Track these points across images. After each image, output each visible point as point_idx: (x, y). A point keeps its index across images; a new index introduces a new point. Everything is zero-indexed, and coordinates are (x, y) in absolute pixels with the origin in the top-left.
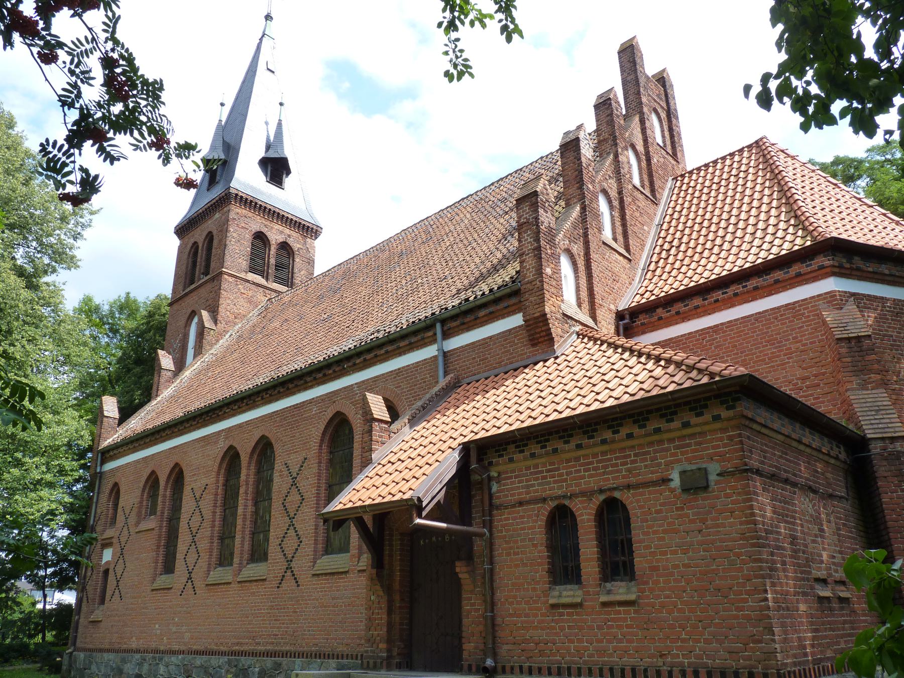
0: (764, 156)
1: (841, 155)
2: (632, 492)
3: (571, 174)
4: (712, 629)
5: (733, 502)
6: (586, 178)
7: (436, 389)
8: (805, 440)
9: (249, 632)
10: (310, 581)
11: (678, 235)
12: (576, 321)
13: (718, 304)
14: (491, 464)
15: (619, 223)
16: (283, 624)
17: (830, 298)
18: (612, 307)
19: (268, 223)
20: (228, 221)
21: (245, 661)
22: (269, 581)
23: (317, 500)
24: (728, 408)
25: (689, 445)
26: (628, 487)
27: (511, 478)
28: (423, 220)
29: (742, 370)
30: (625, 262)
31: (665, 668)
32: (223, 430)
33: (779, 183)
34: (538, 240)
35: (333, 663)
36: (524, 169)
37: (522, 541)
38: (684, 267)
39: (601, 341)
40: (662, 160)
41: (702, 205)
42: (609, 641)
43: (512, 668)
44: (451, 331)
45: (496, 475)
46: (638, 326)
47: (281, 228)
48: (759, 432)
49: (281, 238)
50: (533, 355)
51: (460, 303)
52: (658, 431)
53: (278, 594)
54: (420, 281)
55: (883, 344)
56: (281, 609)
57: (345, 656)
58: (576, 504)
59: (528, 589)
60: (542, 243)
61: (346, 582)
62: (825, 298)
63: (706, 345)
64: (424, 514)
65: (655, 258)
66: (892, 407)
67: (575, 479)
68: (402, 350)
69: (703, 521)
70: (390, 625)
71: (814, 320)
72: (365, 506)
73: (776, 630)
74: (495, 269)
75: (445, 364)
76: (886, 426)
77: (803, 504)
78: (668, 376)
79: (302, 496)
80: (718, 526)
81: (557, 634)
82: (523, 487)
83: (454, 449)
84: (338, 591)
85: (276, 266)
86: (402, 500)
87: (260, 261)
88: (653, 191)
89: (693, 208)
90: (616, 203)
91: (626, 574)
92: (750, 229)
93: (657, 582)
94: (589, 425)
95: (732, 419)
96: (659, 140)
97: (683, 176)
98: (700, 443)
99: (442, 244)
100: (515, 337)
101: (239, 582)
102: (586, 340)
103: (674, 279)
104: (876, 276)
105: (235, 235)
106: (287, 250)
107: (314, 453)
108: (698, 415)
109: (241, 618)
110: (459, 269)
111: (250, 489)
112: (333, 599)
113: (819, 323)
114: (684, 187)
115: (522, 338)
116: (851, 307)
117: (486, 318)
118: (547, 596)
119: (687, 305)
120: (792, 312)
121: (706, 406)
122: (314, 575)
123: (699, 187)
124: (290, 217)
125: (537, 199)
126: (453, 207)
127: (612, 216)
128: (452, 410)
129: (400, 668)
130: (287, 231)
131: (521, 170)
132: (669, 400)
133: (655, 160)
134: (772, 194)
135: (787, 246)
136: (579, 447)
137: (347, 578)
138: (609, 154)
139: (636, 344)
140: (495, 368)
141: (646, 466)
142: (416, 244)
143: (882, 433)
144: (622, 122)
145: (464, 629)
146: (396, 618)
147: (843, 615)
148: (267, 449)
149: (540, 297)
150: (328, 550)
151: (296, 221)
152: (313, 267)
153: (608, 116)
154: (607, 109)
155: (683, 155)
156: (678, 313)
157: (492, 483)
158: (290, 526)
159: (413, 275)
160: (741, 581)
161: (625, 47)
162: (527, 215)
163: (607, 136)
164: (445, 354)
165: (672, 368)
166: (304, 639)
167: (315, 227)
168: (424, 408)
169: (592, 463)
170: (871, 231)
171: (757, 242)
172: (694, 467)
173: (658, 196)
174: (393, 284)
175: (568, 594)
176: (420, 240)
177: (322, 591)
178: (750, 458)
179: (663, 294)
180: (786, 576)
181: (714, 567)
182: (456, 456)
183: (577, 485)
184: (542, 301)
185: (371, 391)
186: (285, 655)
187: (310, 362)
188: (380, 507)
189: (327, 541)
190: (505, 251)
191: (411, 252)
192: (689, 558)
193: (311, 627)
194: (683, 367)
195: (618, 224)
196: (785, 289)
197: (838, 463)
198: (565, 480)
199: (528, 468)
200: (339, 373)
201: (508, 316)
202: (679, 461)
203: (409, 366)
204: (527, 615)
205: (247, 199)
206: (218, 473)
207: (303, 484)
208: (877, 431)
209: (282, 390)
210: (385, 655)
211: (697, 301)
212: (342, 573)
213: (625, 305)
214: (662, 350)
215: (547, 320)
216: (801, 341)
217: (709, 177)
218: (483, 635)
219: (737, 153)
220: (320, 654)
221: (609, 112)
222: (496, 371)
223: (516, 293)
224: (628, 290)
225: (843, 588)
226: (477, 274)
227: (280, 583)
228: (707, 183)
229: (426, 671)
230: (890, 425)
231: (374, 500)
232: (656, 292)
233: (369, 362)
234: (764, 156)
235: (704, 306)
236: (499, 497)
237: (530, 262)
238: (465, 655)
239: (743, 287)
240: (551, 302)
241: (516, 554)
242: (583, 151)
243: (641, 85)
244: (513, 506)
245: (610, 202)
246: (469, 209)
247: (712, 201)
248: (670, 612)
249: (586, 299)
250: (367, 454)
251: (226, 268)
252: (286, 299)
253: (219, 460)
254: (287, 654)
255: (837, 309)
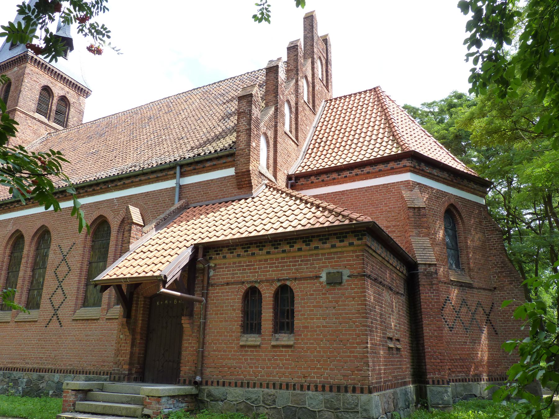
0: (378, 97)
1: (408, 104)
2: (297, 282)
3: (272, 87)
4: (335, 363)
5: (355, 293)
6: (279, 91)
7: (173, 208)
8: (391, 262)
9: (21, 355)
10: (69, 324)
11: (326, 135)
12: (266, 177)
13: (346, 179)
14: (211, 258)
15: (294, 122)
16: (48, 351)
17: (407, 184)
18: (286, 172)
19: (53, 81)
20: (24, 74)
21: (16, 374)
22: (39, 322)
23: (80, 271)
24: (358, 239)
25: (333, 258)
26: (295, 279)
27: (223, 268)
28: (166, 98)
29: (369, 219)
30: (295, 146)
31: (306, 384)
33: (385, 115)
34: (250, 124)
35: (82, 376)
36: (236, 78)
37: (226, 306)
38: (323, 156)
39: (282, 191)
40: (320, 88)
41: (341, 119)
42: (274, 368)
43: (212, 382)
44: (186, 173)
45: (213, 265)
46: (299, 185)
47: (63, 86)
48: (371, 254)
49: (62, 93)
50: (238, 195)
51: (194, 156)
52: (317, 248)
53: (46, 331)
54: (164, 137)
55: (430, 213)
56: (47, 341)
57: (92, 373)
58: (263, 287)
59: (227, 336)
60: (252, 126)
61: (97, 325)
62: (404, 184)
63: (337, 202)
64: (167, 286)
65: (311, 146)
66: (431, 248)
67: (264, 272)
68: (151, 180)
69: (337, 302)
70: (132, 354)
71: (397, 195)
72: (126, 278)
73: (370, 364)
74: (217, 138)
75: (180, 193)
76: (427, 257)
77: (387, 296)
78: (315, 218)
79: (69, 268)
80: (345, 305)
81: (242, 363)
82: (230, 274)
83: (187, 247)
84: (90, 331)
85: (56, 111)
86: (153, 276)
87: (45, 106)
88: (314, 106)
89: (336, 121)
90: (294, 110)
91: (288, 329)
92: (368, 138)
93: (307, 335)
94: (276, 241)
95: (360, 246)
96: (320, 76)
97: (331, 100)
98: (340, 258)
99: (180, 116)
100: (228, 182)
101: (16, 322)
102: (272, 189)
103: (307, 160)
104: (431, 176)
105: (28, 85)
106: (65, 102)
107: (81, 241)
108: (341, 241)
109: (16, 346)
110: (192, 133)
111: (30, 260)
112: (86, 336)
113: (399, 197)
114: (331, 107)
115: (232, 183)
116: (417, 190)
117: (210, 168)
118: (238, 340)
119: (329, 177)
120: (386, 189)
121: (346, 237)
122: (73, 320)
123: (340, 109)
124: (70, 79)
125: (251, 99)
126: (187, 93)
127: (291, 118)
128: (184, 222)
129: (136, 381)
130: (67, 89)
131: (234, 78)
132: (325, 231)
133: (317, 88)
134: (381, 120)
135: (388, 151)
136: (268, 253)
137: (98, 323)
138: (292, 79)
139: (304, 196)
140: (213, 199)
141: (307, 268)
142: (161, 113)
143: (425, 261)
144: (302, 61)
145: (183, 357)
146: (137, 349)
147: (397, 358)
148: (45, 235)
149: (247, 160)
150: (85, 304)
151: (74, 83)
152: (83, 116)
153: (295, 56)
154: (295, 51)
155: (332, 88)
156: (323, 181)
157: (210, 270)
158: (58, 287)
159: (159, 133)
160: (354, 336)
161: (308, 15)
162: (244, 107)
163: (293, 68)
164: (181, 187)
165: (326, 213)
166: (63, 361)
167: (87, 90)
168: (165, 219)
169: (275, 263)
170: (429, 150)
171: (371, 147)
172: (335, 271)
173: (316, 109)
174: (145, 137)
175: (252, 339)
176: (163, 110)
177: (78, 331)
178: (367, 269)
179: (315, 169)
180: (377, 335)
181: (340, 328)
182: (189, 252)
183: (264, 276)
184: (248, 162)
185: (135, 205)
186: (47, 371)
187: (83, 180)
188: (136, 280)
189: (85, 298)
190: (224, 127)
191: (157, 118)
192: (327, 323)
193: (68, 353)
194: (334, 213)
195: (293, 122)
196: (384, 175)
197: (402, 276)
198: (257, 272)
199: (234, 263)
200: (104, 190)
201: (228, 168)
202: (327, 267)
203: (155, 191)
204: (225, 351)
205: (40, 62)
206: (6, 247)
207: (70, 260)
208: (423, 260)
209: (61, 196)
210: (127, 372)
211: (335, 175)
212: (6, 322)
213: (293, 172)
214: (320, 202)
215: (250, 174)
216: (389, 206)
217: (346, 103)
218: (195, 362)
219: (363, 93)
220: (73, 371)
221: (296, 53)
222: (213, 202)
223: (232, 155)
224: (295, 163)
225: (398, 343)
226: (205, 139)
227: (48, 324)
228: (345, 107)
229: (153, 383)
230: (429, 257)
231: (139, 274)
232: (312, 166)
233: (127, 185)
234: (378, 97)
235: (338, 179)
236: (213, 279)
237: (243, 137)
238: (182, 373)
239: (362, 171)
240: (253, 164)
241: (221, 314)
242: (280, 74)
243: (315, 41)
244: (222, 285)
245: (290, 108)
246: (199, 97)
247: (347, 118)
248: (311, 352)
249: (272, 165)
250: (127, 245)
251: (19, 107)
252: (63, 135)
253: (7, 240)
254: (49, 370)
255: (410, 190)
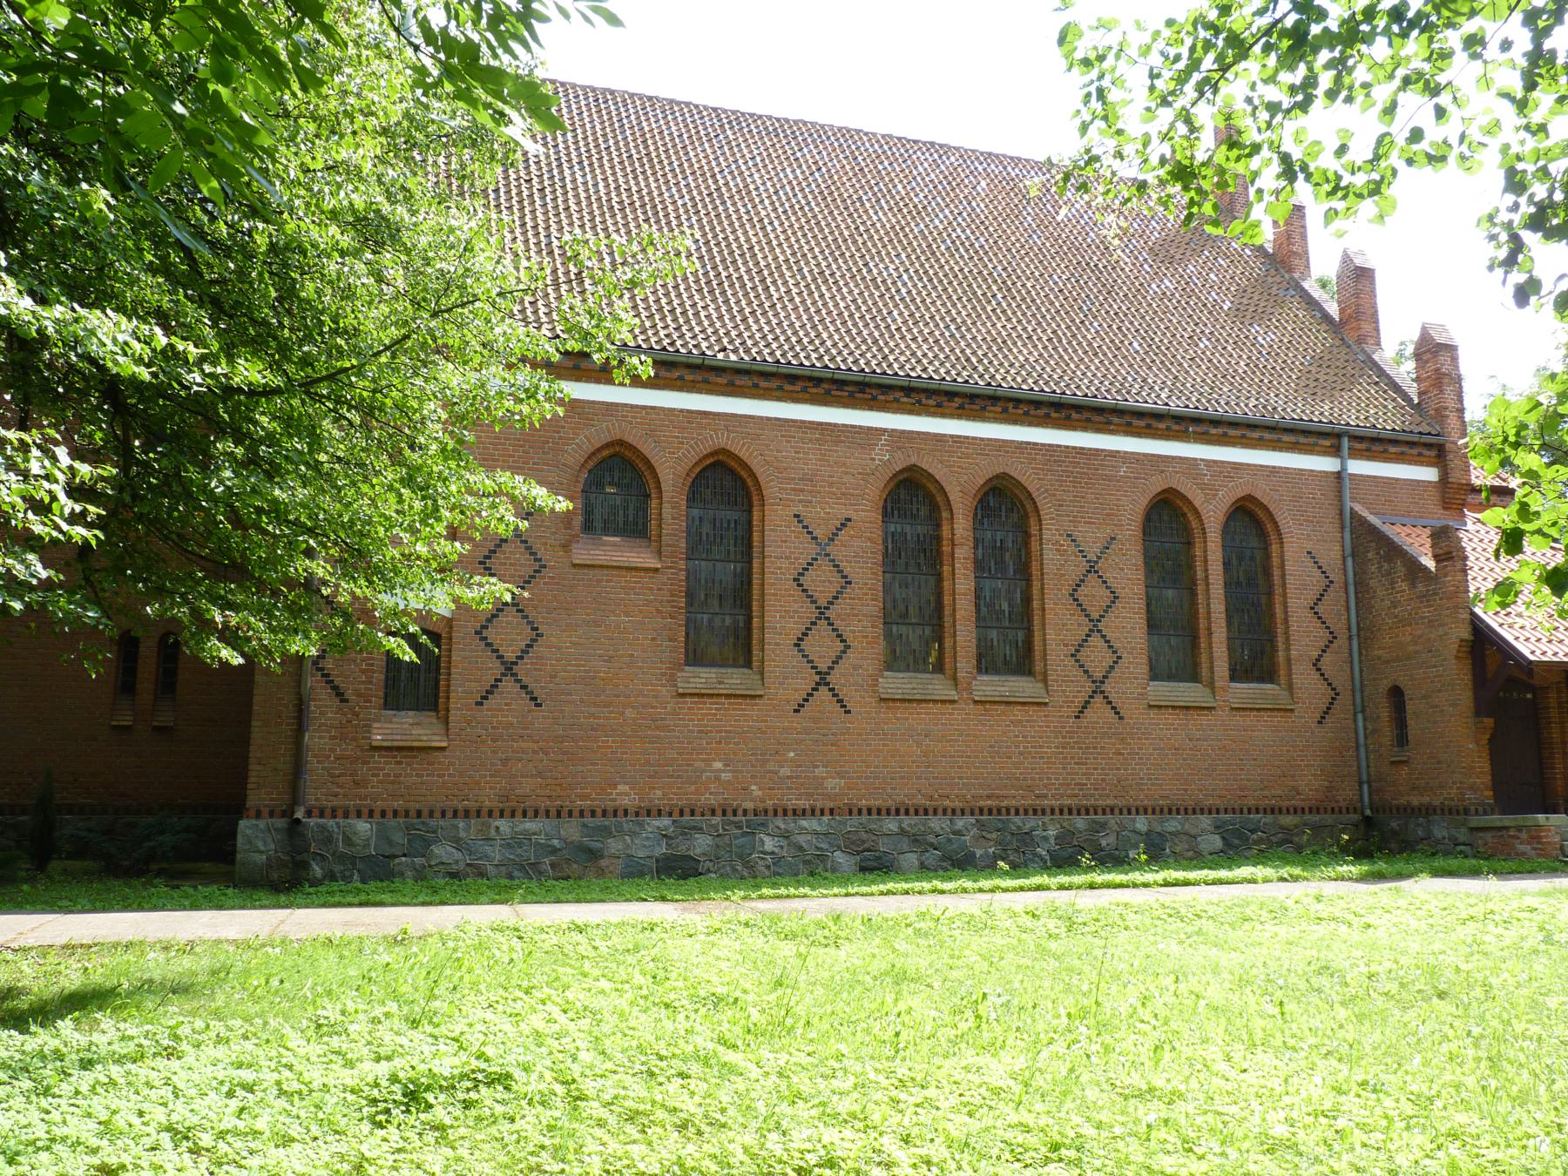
32: (885, 430)
